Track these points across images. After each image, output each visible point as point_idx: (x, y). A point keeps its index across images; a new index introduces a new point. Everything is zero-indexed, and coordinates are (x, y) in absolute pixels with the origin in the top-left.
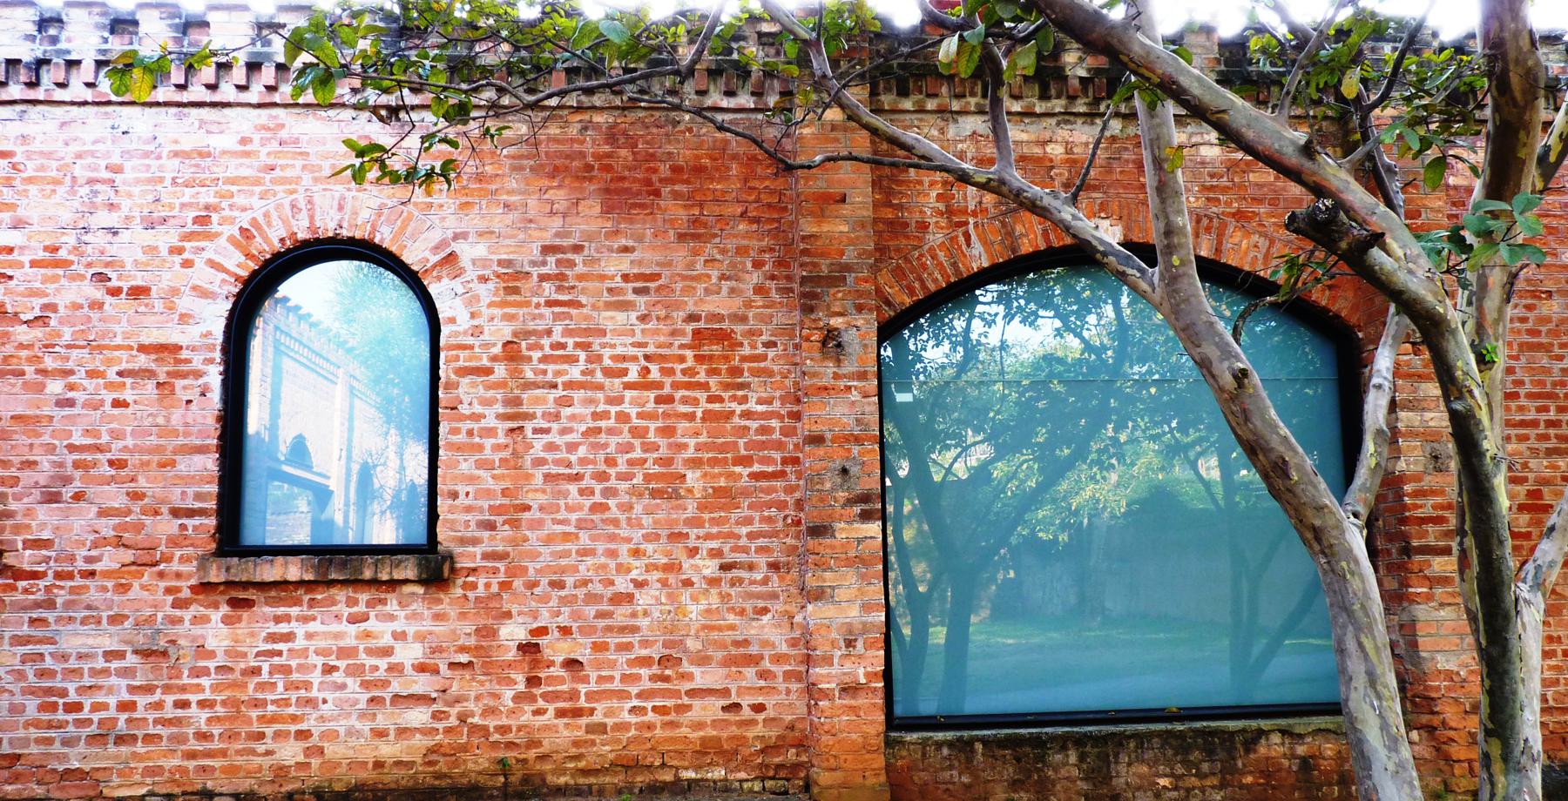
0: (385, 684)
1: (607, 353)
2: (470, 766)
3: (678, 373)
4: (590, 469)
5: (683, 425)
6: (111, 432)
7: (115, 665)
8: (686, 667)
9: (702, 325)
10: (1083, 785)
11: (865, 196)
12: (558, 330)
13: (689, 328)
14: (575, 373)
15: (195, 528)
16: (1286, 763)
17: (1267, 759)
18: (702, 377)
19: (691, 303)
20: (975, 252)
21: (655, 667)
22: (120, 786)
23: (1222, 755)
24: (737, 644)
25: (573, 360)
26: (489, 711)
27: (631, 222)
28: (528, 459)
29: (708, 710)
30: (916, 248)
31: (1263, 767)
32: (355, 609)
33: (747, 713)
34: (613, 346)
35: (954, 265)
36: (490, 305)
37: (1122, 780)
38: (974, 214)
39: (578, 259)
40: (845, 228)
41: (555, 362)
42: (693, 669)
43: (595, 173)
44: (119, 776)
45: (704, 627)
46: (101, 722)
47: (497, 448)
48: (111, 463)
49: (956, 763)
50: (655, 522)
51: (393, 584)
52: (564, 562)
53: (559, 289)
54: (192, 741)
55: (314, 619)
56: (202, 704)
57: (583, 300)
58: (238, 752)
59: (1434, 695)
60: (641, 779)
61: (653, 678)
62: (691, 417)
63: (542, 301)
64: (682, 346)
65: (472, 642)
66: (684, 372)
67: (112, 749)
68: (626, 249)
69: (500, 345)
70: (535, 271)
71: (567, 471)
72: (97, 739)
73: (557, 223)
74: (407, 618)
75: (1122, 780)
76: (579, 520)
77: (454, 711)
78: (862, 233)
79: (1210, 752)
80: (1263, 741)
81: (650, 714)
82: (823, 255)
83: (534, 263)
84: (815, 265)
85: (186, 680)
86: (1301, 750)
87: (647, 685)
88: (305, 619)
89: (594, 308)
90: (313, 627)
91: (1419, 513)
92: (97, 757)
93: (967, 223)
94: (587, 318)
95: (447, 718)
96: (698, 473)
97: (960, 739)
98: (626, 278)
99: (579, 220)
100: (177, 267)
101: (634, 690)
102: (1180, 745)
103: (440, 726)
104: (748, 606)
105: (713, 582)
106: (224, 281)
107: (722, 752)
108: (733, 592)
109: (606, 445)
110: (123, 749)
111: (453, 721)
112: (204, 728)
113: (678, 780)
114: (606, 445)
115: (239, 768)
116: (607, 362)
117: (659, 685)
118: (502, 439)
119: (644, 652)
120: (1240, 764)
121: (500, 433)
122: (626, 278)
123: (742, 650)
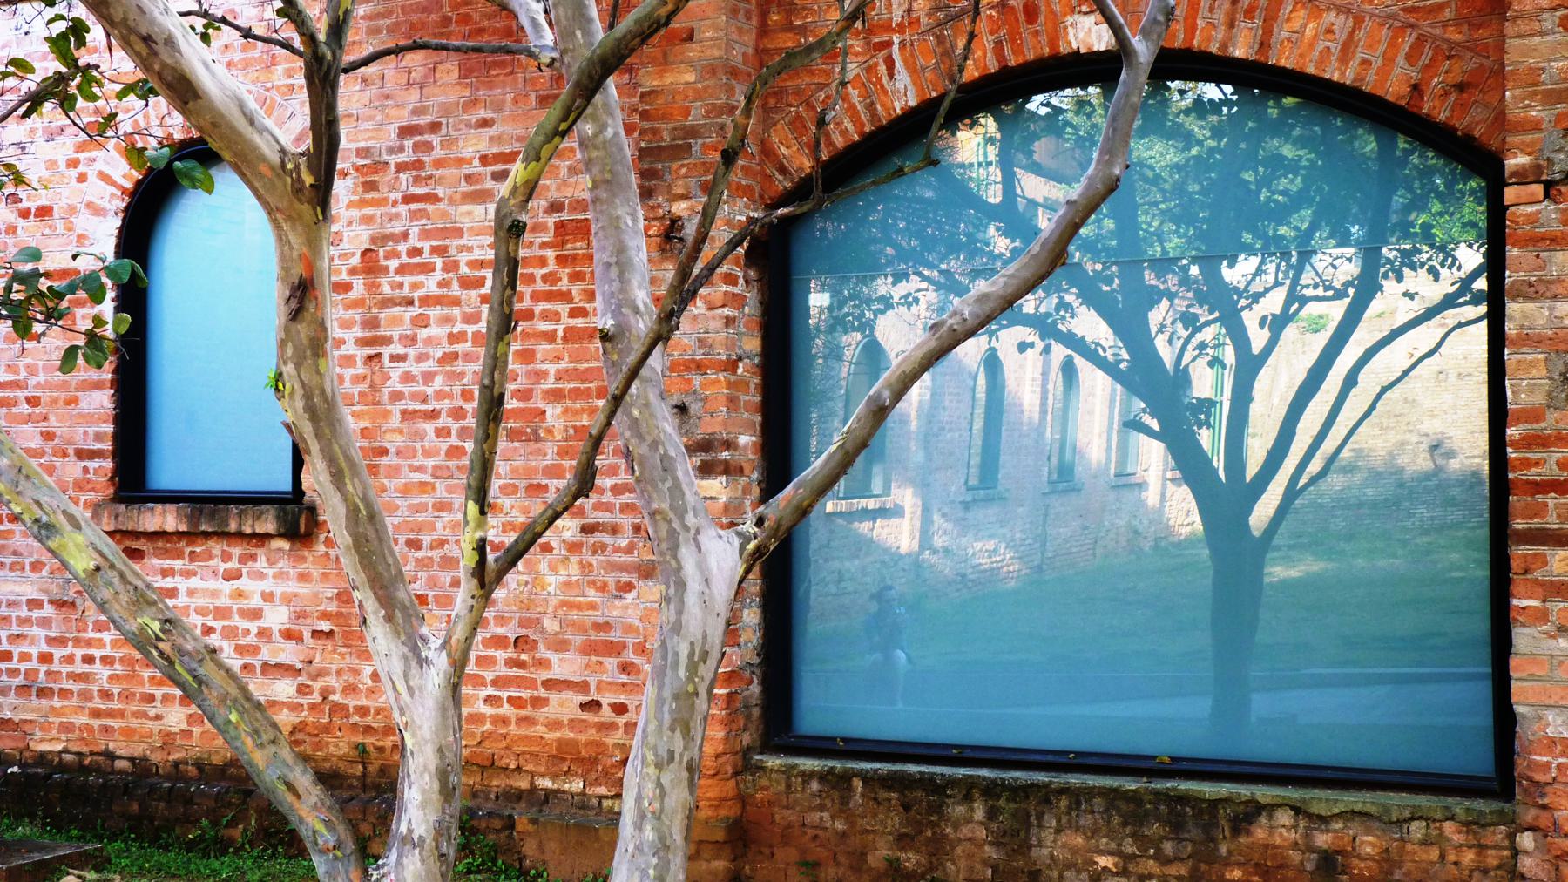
0: (255, 650)
1: (464, 258)
2: (332, 749)
3: (539, 280)
4: (445, 406)
5: (543, 347)
6: (27, 366)
7: (36, 614)
8: (543, 652)
9: (565, 216)
10: (990, 852)
11: (716, 28)
12: (414, 231)
13: (551, 220)
14: (431, 285)
15: (96, 470)
16: (1296, 857)
17: (1266, 846)
18: (563, 285)
19: (553, 188)
20: (900, 85)
21: (511, 649)
22: (42, 740)
23: (1195, 832)
24: (598, 627)
25: (428, 269)
26: (350, 689)
27: (490, 86)
28: (385, 391)
29: (564, 706)
30: (822, 86)
31: (1256, 857)
32: (229, 565)
33: (607, 714)
34: (470, 249)
35: (871, 107)
36: (350, 205)
37: (1046, 852)
38: (901, 28)
39: (434, 139)
40: (691, 77)
41: (411, 273)
42: (550, 655)
43: (453, 27)
44: (42, 729)
45: (563, 604)
46: (27, 671)
47: (357, 379)
48: (28, 400)
49: (829, 805)
50: (514, 471)
51: (263, 538)
52: (421, 518)
53: (417, 180)
54: (97, 699)
55: (195, 574)
56: (107, 660)
57: (440, 191)
58: (134, 714)
59: (1538, 777)
60: (498, 783)
61: (512, 663)
62: (550, 337)
63: (399, 196)
64: (544, 245)
65: (333, 607)
66: (545, 278)
67: (35, 702)
68: (485, 123)
69: (358, 255)
70: (393, 160)
71: (423, 407)
72: (23, 690)
73: (413, 96)
74: (274, 577)
75: (1046, 852)
76: (435, 467)
77: (317, 685)
78: (711, 82)
79: (1176, 827)
80: (1263, 820)
81: (506, 705)
82: (664, 117)
83: (391, 150)
84: (655, 132)
85: (91, 635)
86: (1322, 840)
87: (502, 670)
88: (188, 574)
89: (452, 201)
90: (194, 582)
91: (1532, 474)
92: (25, 709)
93: (889, 44)
94: (444, 214)
95: (311, 693)
96: (559, 409)
97: (831, 770)
98: (484, 160)
99: (437, 90)
100: (74, 182)
101: (489, 676)
102: (1132, 811)
103: (305, 701)
104: (610, 579)
105: (574, 547)
106: (112, 195)
107: (579, 760)
108: (594, 560)
109: (462, 375)
110: (44, 702)
111: (316, 698)
112: (106, 686)
113: (533, 789)
114: (462, 375)
115: (133, 731)
116: (464, 270)
117: (515, 672)
118: (360, 369)
119: (500, 631)
120: (1223, 850)
121: (359, 361)
122: (484, 160)
123: (602, 636)
